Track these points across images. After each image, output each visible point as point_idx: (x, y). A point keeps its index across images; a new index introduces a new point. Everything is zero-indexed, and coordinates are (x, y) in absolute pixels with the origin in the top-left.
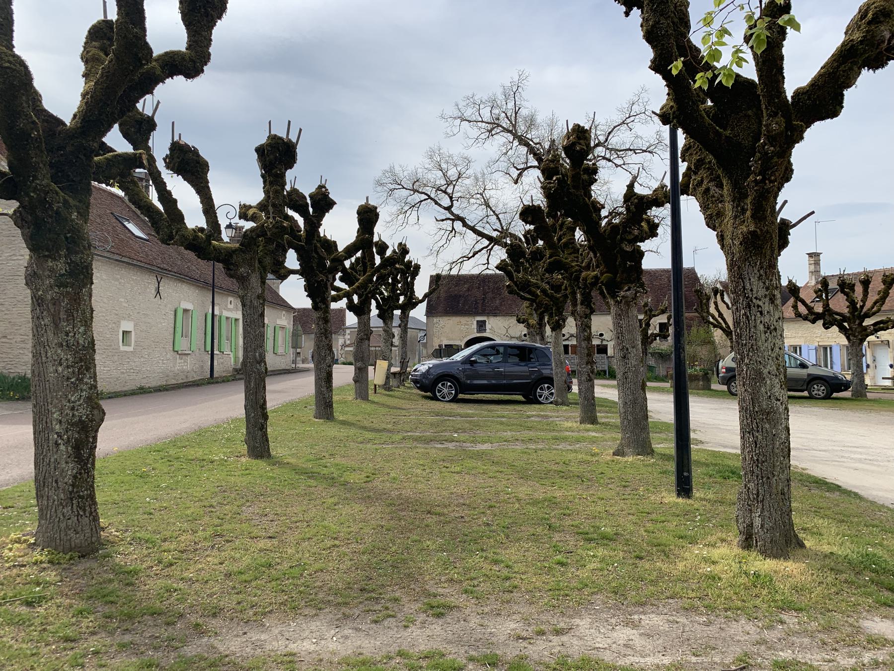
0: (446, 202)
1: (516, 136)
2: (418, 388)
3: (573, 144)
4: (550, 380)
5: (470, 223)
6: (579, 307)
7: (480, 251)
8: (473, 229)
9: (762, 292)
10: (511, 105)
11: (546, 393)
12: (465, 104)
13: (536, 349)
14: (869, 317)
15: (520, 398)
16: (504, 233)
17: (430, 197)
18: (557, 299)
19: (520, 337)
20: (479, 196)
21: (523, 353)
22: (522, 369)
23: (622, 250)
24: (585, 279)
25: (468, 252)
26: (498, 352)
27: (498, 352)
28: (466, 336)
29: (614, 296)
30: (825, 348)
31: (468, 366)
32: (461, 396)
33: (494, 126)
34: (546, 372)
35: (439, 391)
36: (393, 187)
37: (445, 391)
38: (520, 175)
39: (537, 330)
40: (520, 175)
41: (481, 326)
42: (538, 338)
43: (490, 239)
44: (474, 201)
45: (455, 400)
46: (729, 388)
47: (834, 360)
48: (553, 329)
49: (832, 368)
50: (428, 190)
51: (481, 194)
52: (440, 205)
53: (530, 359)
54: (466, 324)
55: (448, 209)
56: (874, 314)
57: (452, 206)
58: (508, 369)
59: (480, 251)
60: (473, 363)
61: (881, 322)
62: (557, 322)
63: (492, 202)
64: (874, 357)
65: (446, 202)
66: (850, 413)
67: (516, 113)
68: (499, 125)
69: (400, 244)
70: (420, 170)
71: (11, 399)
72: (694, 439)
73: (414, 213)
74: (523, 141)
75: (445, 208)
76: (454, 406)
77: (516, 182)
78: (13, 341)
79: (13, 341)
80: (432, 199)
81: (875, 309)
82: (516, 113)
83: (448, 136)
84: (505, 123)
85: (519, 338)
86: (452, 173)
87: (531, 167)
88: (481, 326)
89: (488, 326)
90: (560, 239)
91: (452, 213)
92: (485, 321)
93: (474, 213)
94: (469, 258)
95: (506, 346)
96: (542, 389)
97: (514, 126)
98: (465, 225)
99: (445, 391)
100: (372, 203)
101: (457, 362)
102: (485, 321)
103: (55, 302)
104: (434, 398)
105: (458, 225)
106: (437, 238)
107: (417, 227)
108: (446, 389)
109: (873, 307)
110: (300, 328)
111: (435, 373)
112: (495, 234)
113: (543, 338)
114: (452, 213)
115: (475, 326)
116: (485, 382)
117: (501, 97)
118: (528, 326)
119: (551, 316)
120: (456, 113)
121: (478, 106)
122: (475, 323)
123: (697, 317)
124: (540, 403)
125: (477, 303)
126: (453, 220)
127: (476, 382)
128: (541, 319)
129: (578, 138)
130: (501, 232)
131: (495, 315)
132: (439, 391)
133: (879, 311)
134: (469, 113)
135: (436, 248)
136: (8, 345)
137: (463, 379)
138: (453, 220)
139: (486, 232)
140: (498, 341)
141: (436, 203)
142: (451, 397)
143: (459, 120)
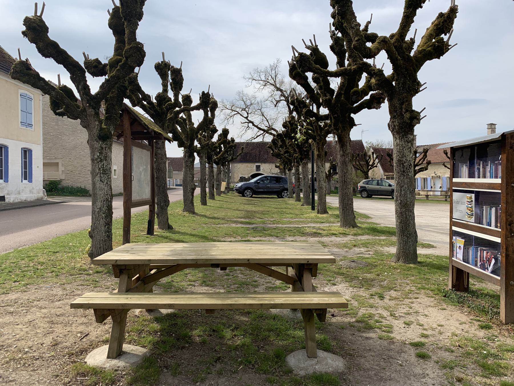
0: (245, 115)
1: (275, 86)
2: (238, 192)
3: (291, 121)
4: (287, 190)
5: (255, 124)
6: (295, 164)
7: (259, 135)
8: (257, 127)
9: (320, 165)
10: (273, 72)
11: (286, 194)
12: (254, 72)
13: (282, 178)
14: (418, 166)
15: (276, 196)
16: (271, 128)
17: (238, 113)
18: (290, 159)
19: (277, 173)
20: (259, 111)
21: (277, 179)
22: (277, 185)
23: (303, 150)
24: (294, 157)
25: (254, 135)
26: (268, 179)
27: (268, 179)
28: (250, 173)
29: (302, 162)
30: (424, 179)
31: (256, 184)
32: (254, 196)
33: (266, 83)
34: (286, 186)
35: (246, 194)
36: (222, 108)
37: (248, 193)
38: (277, 103)
39: (283, 171)
40: (277, 103)
41: (258, 168)
42: (283, 174)
43: (264, 130)
44: (257, 113)
45: (251, 197)
46: (361, 195)
47: (418, 185)
48: (288, 171)
49: (427, 188)
50: (238, 110)
51: (260, 110)
52: (243, 116)
53: (280, 182)
54: (250, 167)
55: (246, 118)
56: (420, 165)
57: (248, 117)
58: (271, 185)
59: (259, 135)
60: (258, 183)
61: (422, 168)
62: (290, 168)
63: (265, 114)
64: (434, 183)
65: (245, 115)
66: (390, 202)
67: (276, 76)
68: (268, 82)
69: (232, 138)
70: (234, 101)
71: (79, 196)
72: (419, 254)
73: (232, 119)
74: (278, 89)
75: (245, 118)
76: (251, 198)
77: (275, 106)
78: (75, 174)
79: (75, 174)
80: (239, 114)
81: (420, 162)
82: (276, 76)
83: (246, 86)
84: (272, 82)
85: (277, 174)
86: (248, 103)
87: (282, 100)
88: (258, 168)
89: (261, 168)
90: (288, 143)
91: (248, 120)
92: (260, 166)
93: (256, 119)
94: (255, 139)
95: (271, 177)
96: (284, 193)
97: (275, 82)
98: (253, 125)
99: (248, 193)
100: (227, 128)
101: (252, 183)
102: (260, 166)
103: (190, 166)
104: (244, 196)
105: (250, 125)
106: (241, 130)
107: (232, 125)
108: (248, 193)
109: (419, 162)
110: (172, 168)
111: (244, 187)
112: (266, 128)
113: (285, 174)
114: (248, 120)
115: (255, 168)
116: (262, 190)
117: (269, 70)
118: (280, 169)
119: (288, 166)
120: (250, 77)
121: (259, 72)
122: (255, 166)
123: (365, 164)
124: (283, 198)
125: (256, 156)
126: (248, 123)
127: (259, 190)
128: (285, 166)
129: (292, 119)
130: (269, 128)
131: (265, 163)
132: (246, 194)
133: (422, 163)
134: (256, 76)
135: (241, 134)
136: (73, 175)
137: (254, 188)
138: (248, 123)
139: (262, 128)
140: (266, 175)
141: (241, 115)
142: (250, 196)
143: (250, 80)
